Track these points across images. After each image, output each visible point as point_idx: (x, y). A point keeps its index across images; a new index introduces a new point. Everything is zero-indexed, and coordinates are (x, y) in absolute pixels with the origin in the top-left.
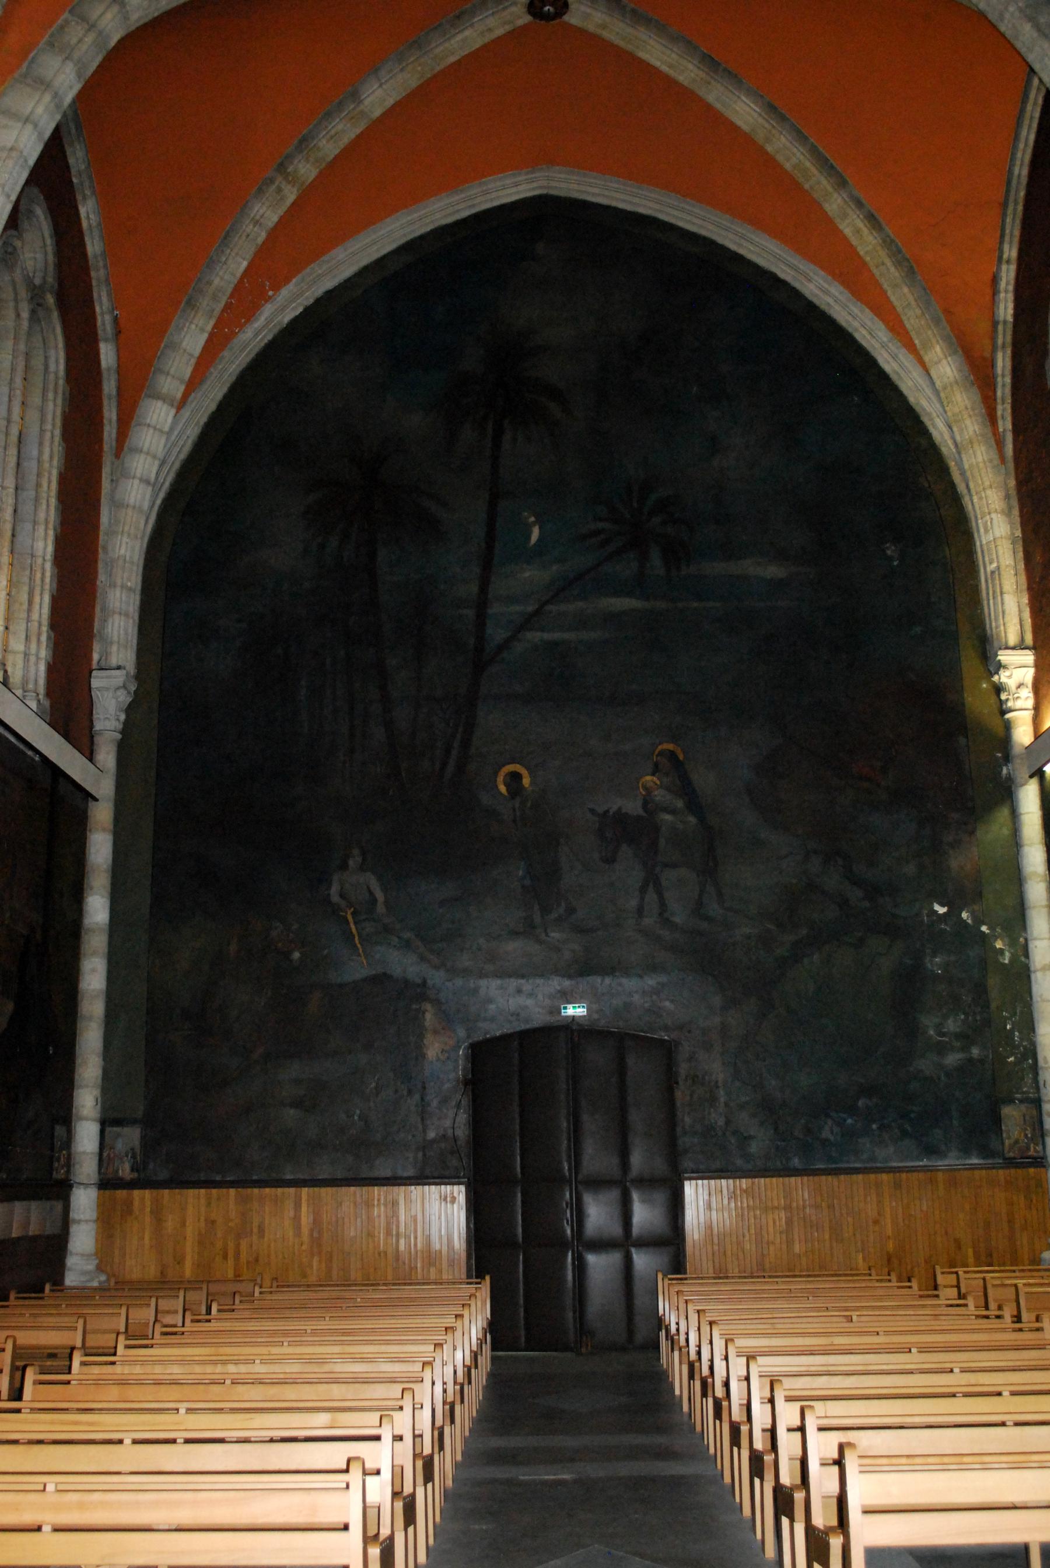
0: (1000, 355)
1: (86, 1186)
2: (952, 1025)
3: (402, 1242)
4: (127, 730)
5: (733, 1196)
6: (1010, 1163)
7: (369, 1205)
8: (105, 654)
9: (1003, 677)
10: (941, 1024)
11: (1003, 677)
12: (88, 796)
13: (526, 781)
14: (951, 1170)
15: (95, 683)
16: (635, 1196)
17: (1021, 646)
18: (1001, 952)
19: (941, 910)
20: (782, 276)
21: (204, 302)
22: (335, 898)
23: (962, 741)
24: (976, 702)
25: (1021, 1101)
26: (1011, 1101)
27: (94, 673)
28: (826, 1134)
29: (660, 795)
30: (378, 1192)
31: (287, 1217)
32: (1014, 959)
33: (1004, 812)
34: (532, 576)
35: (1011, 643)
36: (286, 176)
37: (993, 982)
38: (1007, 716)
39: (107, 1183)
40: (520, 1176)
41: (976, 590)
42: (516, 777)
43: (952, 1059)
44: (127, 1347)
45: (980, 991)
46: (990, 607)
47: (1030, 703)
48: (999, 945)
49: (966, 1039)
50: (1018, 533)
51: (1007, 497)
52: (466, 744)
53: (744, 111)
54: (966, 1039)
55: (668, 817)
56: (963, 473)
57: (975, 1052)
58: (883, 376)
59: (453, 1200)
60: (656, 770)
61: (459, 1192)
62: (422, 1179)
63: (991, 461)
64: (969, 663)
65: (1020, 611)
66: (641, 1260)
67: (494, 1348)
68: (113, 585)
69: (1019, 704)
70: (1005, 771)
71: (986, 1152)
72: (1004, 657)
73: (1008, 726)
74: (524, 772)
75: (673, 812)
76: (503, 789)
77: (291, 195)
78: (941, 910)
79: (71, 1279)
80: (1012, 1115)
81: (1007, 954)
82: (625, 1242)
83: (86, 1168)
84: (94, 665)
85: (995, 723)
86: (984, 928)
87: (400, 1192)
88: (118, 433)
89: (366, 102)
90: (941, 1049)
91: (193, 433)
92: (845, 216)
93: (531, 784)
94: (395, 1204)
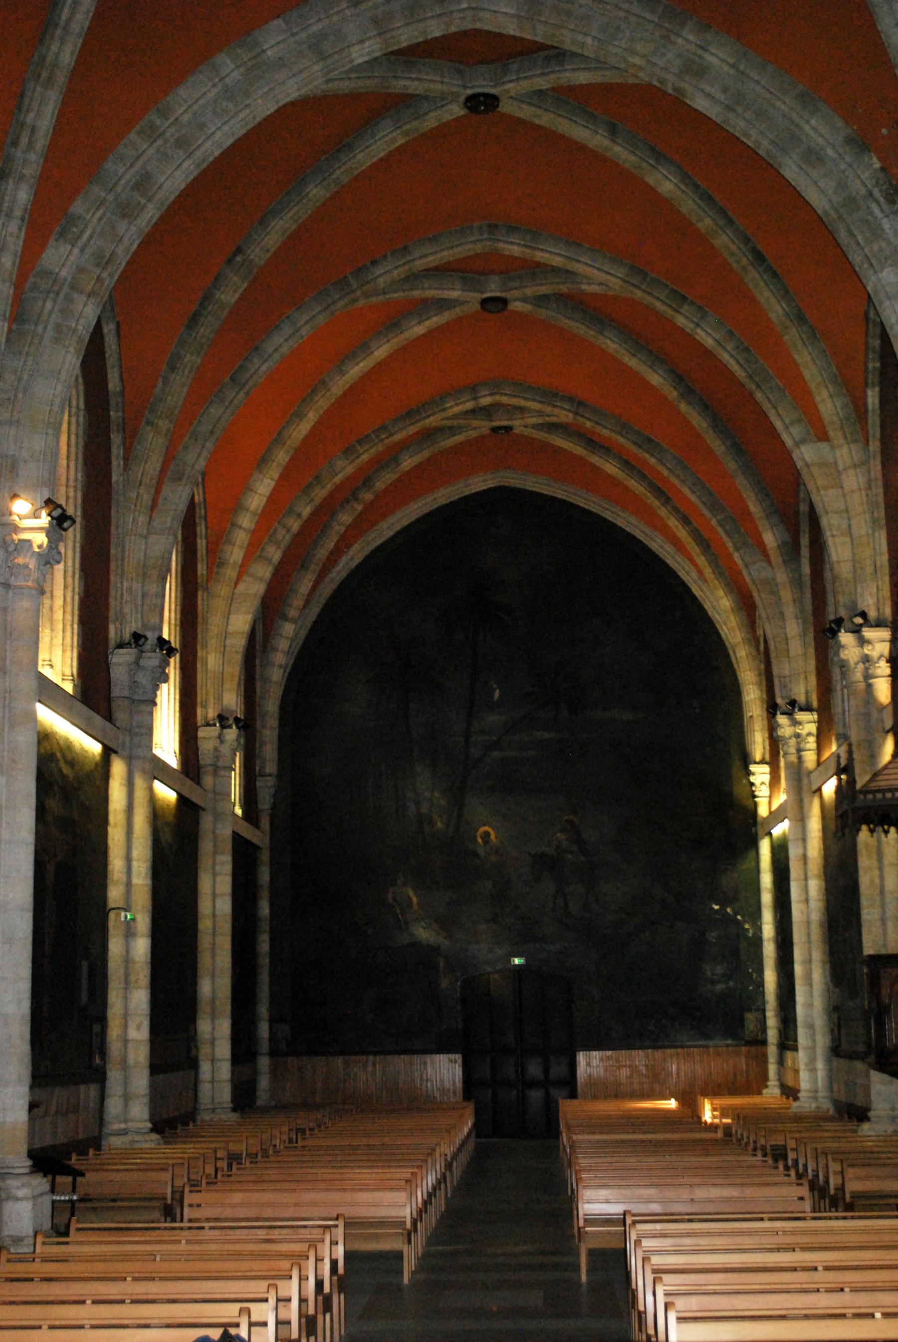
0: (870, 393)
1: (265, 1055)
2: (719, 970)
3: (429, 1084)
4: (274, 807)
5: (601, 1060)
6: (749, 1043)
7: (411, 1064)
8: (263, 767)
9: (752, 779)
10: (713, 970)
11: (752, 779)
12: (257, 848)
13: (492, 837)
14: (716, 1046)
15: (258, 784)
16: (552, 1058)
17: (762, 762)
18: (748, 930)
19: (716, 907)
20: (638, 536)
21: (312, 567)
22: (390, 901)
23: (731, 812)
24: (739, 791)
25: (756, 1010)
26: (750, 1010)
27: (258, 778)
28: (651, 1027)
29: (565, 844)
30: (416, 1058)
31: (367, 1073)
32: (754, 934)
33: (752, 853)
34: (493, 719)
35: (758, 760)
36: (356, 499)
37: (743, 946)
38: (756, 799)
39: (273, 1053)
40: (238, 754)
41: (741, 727)
42: (487, 834)
43: (720, 987)
44: (44, 1243)
45: (736, 953)
46: (748, 736)
47: (767, 793)
48: (747, 926)
49: (727, 977)
50: (765, 696)
51: (760, 675)
52: (460, 816)
53: (666, 183)
54: (727, 977)
55: (570, 856)
56: (736, 658)
57: (731, 984)
58: (694, 598)
59: (456, 1062)
60: (562, 831)
61: (458, 1057)
62: (440, 1050)
63: (751, 654)
64: (737, 764)
65: (764, 741)
66: (553, 1091)
67: (476, 1137)
68: (264, 727)
69: (808, 746)
70: (754, 829)
71: (735, 1036)
72: (753, 768)
73: (756, 805)
74: (492, 832)
75: (572, 853)
76: (480, 840)
77: (359, 508)
78: (716, 907)
79: (260, 1103)
80: (750, 1017)
81: (751, 931)
82: (545, 1084)
83: (264, 1046)
84: (257, 773)
85: (749, 803)
86: (739, 917)
87: (428, 1058)
88: (194, 512)
89: (402, 465)
90: (713, 982)
91: (303, 633)
92: (669, 518)
93: (496, 838)
94: (425, 1064)
